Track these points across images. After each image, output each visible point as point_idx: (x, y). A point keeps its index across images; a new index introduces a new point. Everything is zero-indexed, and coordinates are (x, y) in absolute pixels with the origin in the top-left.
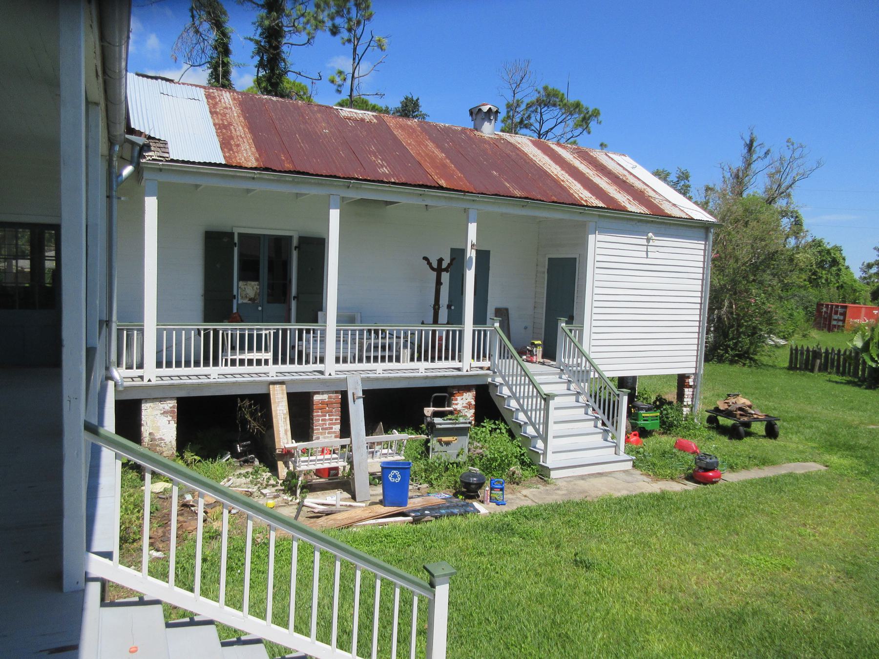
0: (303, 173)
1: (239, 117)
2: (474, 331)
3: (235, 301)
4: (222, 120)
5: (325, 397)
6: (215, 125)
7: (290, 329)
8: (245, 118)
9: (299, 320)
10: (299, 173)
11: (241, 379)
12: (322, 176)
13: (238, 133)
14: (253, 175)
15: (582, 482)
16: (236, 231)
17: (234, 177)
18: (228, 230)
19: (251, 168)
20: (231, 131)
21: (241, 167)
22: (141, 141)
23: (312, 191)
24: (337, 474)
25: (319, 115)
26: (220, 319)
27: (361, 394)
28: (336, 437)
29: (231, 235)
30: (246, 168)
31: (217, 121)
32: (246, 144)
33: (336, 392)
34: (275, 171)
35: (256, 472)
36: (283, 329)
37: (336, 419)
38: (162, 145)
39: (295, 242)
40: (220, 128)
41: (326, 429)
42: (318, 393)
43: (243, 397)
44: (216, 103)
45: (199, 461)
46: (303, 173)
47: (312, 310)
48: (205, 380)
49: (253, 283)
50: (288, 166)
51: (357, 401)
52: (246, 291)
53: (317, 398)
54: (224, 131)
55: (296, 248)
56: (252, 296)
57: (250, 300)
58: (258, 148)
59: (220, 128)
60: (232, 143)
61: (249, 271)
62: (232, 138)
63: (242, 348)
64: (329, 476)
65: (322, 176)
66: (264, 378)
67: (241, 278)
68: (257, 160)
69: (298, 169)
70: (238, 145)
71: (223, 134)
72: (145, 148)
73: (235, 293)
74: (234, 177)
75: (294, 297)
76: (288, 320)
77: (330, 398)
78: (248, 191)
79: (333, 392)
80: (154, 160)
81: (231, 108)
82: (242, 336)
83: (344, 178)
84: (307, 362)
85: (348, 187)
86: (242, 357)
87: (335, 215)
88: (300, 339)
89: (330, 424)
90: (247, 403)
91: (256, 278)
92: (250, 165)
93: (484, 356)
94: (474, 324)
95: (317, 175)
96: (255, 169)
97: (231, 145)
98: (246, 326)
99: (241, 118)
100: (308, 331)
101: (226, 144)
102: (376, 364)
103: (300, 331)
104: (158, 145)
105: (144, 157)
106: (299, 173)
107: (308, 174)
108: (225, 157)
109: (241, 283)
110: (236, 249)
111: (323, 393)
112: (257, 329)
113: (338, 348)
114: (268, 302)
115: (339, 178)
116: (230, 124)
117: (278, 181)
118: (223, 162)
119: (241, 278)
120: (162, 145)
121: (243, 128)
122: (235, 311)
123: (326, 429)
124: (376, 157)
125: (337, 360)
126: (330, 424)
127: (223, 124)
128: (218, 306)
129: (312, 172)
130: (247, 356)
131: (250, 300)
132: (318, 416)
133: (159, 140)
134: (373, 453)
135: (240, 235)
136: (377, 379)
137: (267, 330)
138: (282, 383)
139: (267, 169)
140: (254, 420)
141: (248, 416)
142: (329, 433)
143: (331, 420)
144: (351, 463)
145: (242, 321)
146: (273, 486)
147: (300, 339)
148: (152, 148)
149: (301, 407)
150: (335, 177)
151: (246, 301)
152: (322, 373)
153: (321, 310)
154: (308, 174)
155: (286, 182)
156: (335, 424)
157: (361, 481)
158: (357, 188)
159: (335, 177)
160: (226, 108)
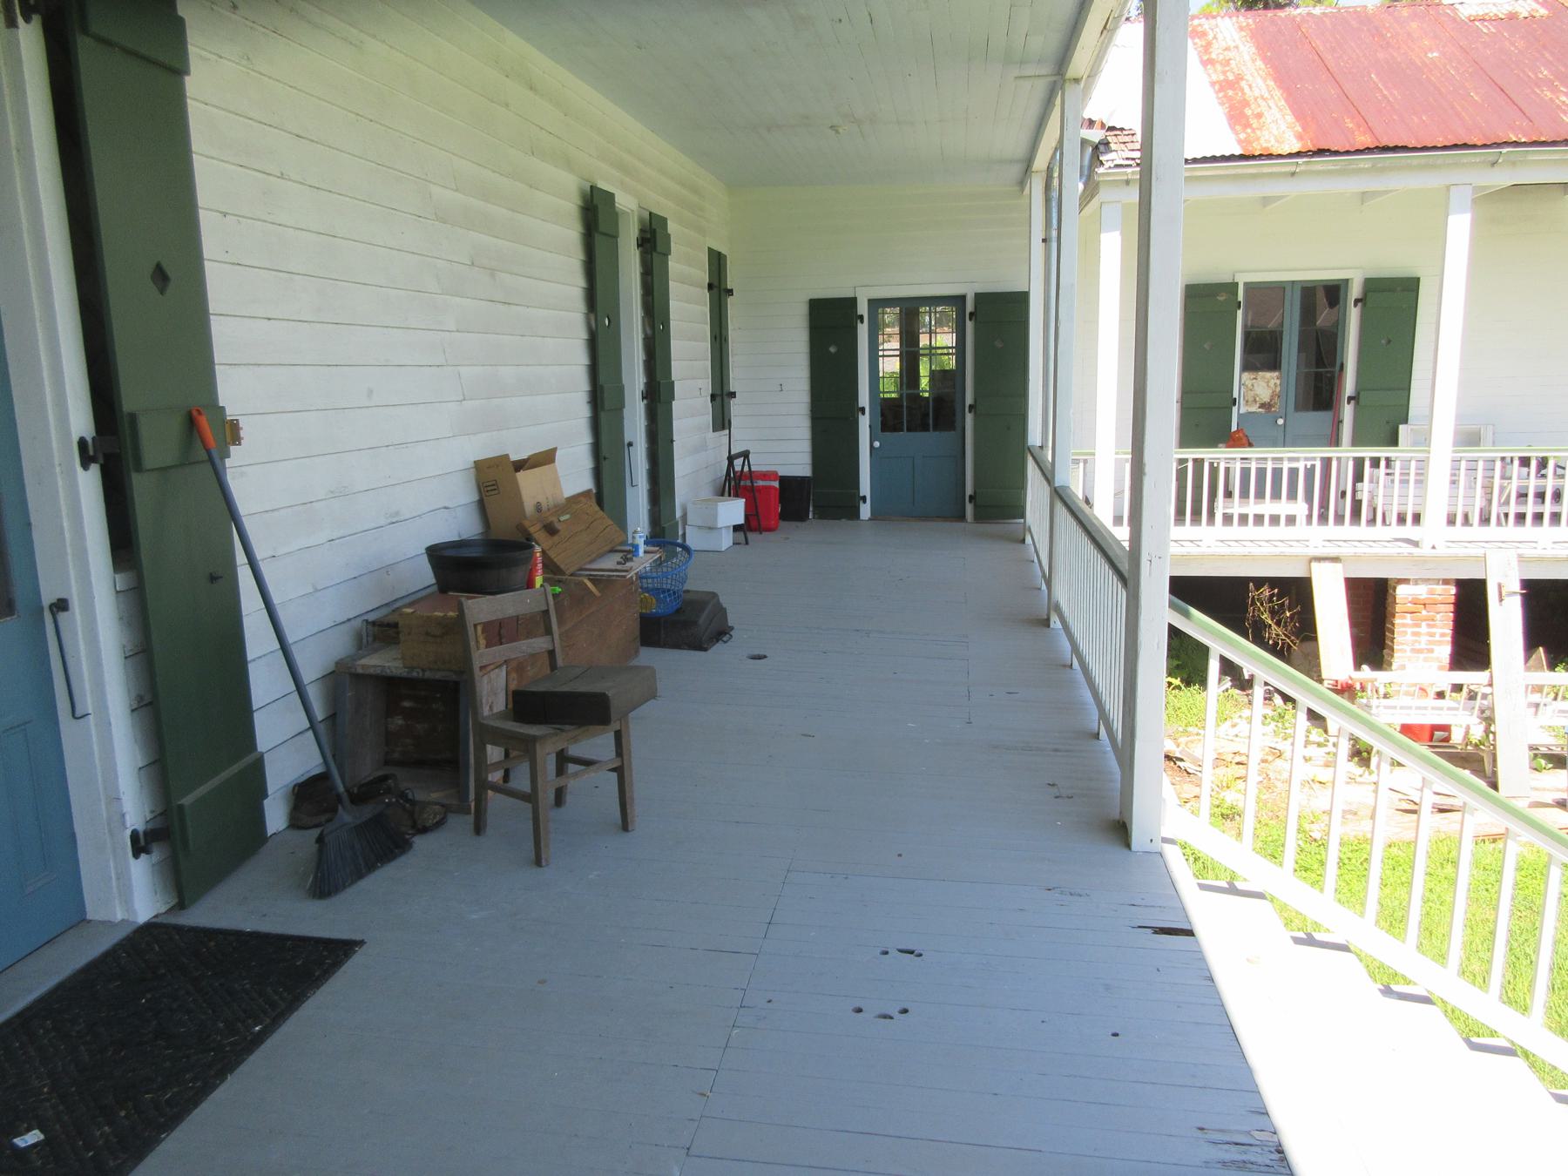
0: (1395, 149)
1: (1254, 61)
2: (1456, 461)
3: (1235, 409)
4: (1224, 73)
5: (1421, 591)
6: (1213, 84)
7: (1339, 459)
8: (1264, 59)
9: (1357, 441)
10: (1386, 149)
11: (1256, 551)
12: (1435, 148)
13: (1257, 93)
14: (1292, 169)
15: (127, 817)
16: (1241, 280)
17: (1254, 176)
18: (1227, 279)
19: (1290, 155)
20: (1242, 90)
21: (1270, 156)
22: (1095, 135)
23: (1405, 181)
24: (1447, 739)
25: (1414, 25)
26: (1212, 442)
27: (1517, 587)
28: (1441, 668)
29: (1233, 286)
30: (1280, 156)
31: (1215, 78)
32: (1275, 110)
33: (1446, 582)
34: (1337, 153)
35: (1281, 716)
36: (1195, 460)
37: (1443, 635)
38: (1127, 139)
39: (1355, 291)
40: (1221, 89)
41: (1419, 651)
42: (1405, 581)
43: (1260, 582)
44: (1209, 44)
45: (1179, 688)
46: (1395, 149)
47: (1386, 419)
48: (1193, 550)
49: (1268, 375)
50: (1364, 140)
51: (1507, 600)
52: (1255, 389)
53: (1402, 592)
54: (1230, 93)
55: (1357, 301)
56: (1267, 399)
57: (1262, 406)
58: (1299, 115)
59: (1221, 89)
60: (1248, 112)
61: (1263, 351)
62: (1246, 104)
63: (1245, 494)
64: (1431, 739)
65: (1435, 148)
66: (1299, 550)
67: (1247, 367)
68: (1300, 137)
69: (1385, 142)
70: (1259, 116)
71: (1230, 99)
72: (1102, 148)
73: (1235, 395)
74: (1254, 176)
75: (1350, 399)
76: (1335, 441)
77: (1431, 592)
78: (1266, 201)
79: (1437, 581)
80: (1117, 166)
81: (1237, 47)
82: (1245, 473)
83: (1485, 146)
84: (1372, 522)
85: (1493, 164)
86: (1244, 511)
87: (1460, 226)
88: (1359, 477)
89: (1430, 642)
90: (1266, 592)
91: (1274, 365)
92: (1286, 150)
93: (1196, 513)
94: (1455, 444)
95: (1425, 149)
96: (1298, 154)
97: (1247, 117)
98: (1252, 453)
99: (1259, 63)
100: (1375, 463)
101: (1238, 115)
102: (1537, 529)
103: (1359, 463)
104: (1121, 139)
105: (1102, 163)
106: (1386, 149)
107: (1405, 148)
108: (1240, 142)
109: (1246, 375)
110: (1240, 313)
111: (1416, 582)
112: (1291, 459)
113: (1453, 497)
114: (1297, 409)
115: (1474, 147)
116: (1239, 78)
117: (1342, 172)
118: (1238, 152)
119: (1247, 367)
120: (1127, 139)
121: (1264, 80)
122: (1234, 428)
123: (1419, 651)
124: (1555, 90)
125: (1451, 521)
126: (1430, 642)
127: (1227, 81)
128: (1206, 418)
129: (1475, 141)
130: (1252, 508)
131: (1262, 406)
132: (1404, 625)
133: (1122, 129)
134: (1537, 706)
135: (1250, 287)
136: (1540, 560)
137: (1304, 457)
138: (1335, 559)
139: (1321, 152)
140: (1278, 624)
141: (1266, 617)
142: (1426, 660)
143: (1432, 635)
144: (1489, 720)
145: (1250, 445)
146: (1319, 745)
147: (1359, 477)
148: (1113, 146)
149: (1373, 605)
150: (1465, 146)
151: (1254, 408)
152: (1416, 544)
153: (1405, 421)
154: (1405, 148)
155: (1359, 171)
156: (1440, 643)
157: (1512, 762)
158: (1514, 164)
159: (1465, 146)
160: (1227, 49)
